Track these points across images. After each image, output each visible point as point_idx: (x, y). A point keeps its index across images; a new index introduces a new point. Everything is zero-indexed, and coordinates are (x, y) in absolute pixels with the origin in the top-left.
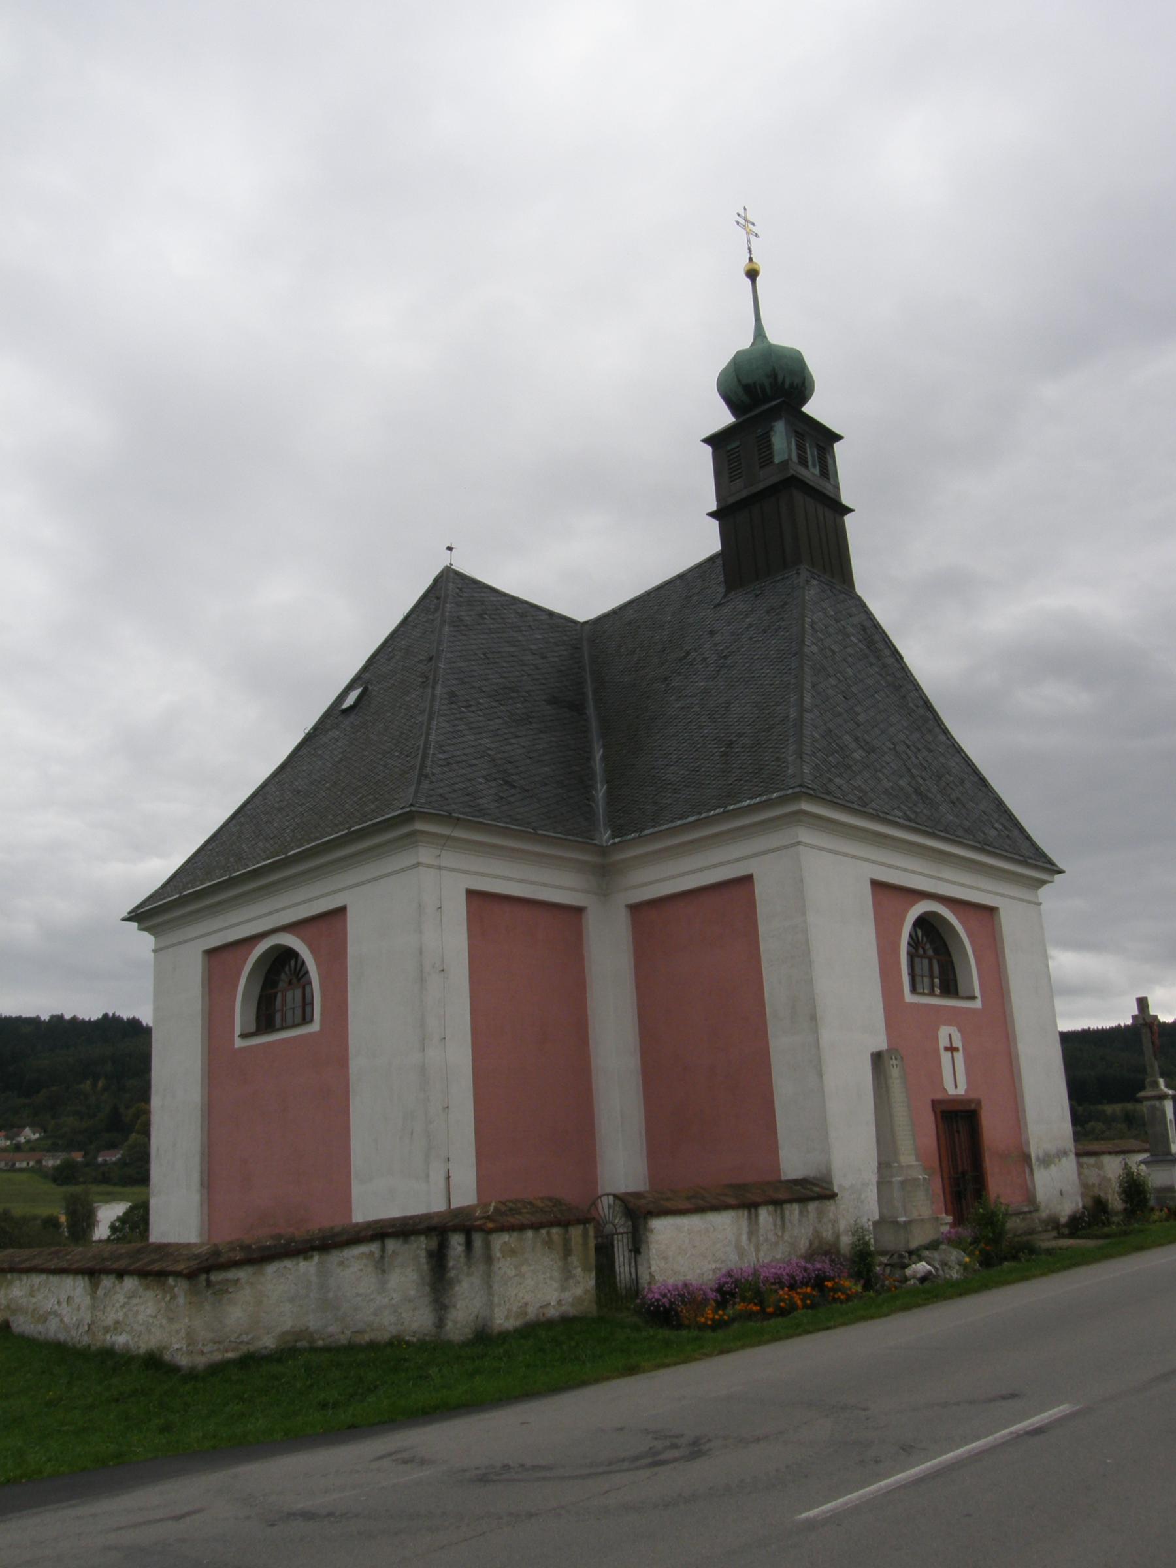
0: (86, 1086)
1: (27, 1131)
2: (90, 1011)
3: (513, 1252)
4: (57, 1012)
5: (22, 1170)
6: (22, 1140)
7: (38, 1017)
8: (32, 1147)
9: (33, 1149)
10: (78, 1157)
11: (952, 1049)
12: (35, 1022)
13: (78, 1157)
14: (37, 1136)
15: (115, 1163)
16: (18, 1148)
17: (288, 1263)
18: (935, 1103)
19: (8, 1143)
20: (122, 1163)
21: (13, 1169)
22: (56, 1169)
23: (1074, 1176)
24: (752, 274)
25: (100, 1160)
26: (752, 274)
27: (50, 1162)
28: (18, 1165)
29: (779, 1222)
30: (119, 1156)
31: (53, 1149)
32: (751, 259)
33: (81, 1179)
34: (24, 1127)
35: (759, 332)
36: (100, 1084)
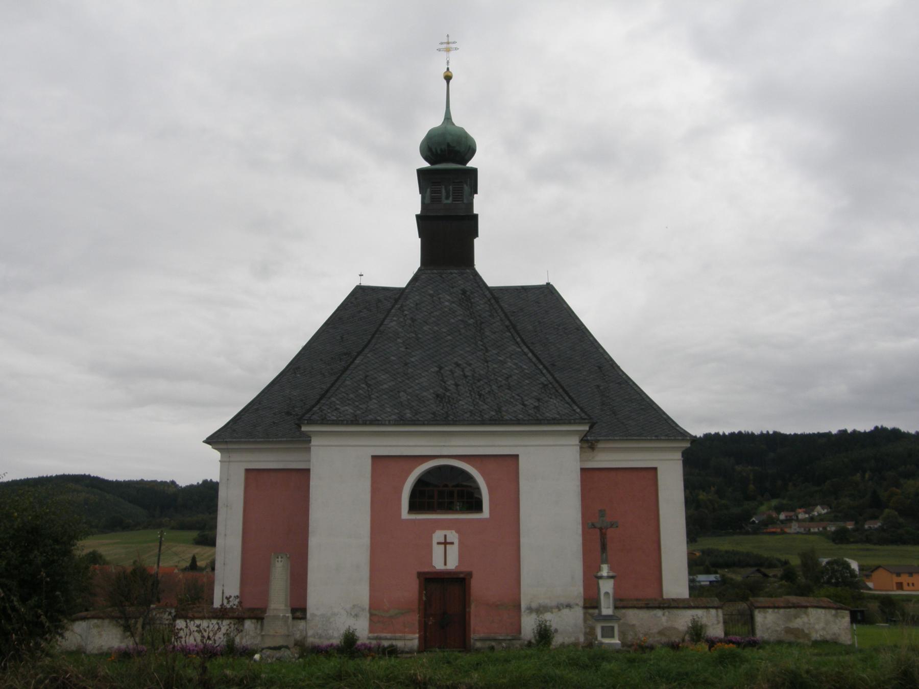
0: (858, 477)
1: (819, 508)
2: (865, 426)
3: (98, 626)
4: (842, 428)
5: (815, 533)
6: (816, 513)
7: (830, 432)
8: (821, 518)
9: (822, 520)
10: (850, 526)
11: (445, 543)
12: (828, 435)
13: (850, 526)
14: (825, 511)
15: (876, 529)
16: (812, 519)
17: (80, 622)
18: (420, 575)
19: (807, 516)
20: (881, 529)
21: (809, 533)
22: (833, 533)
23: (580, 621)
24: (448, 78)
25: (866, 527)
26: (448, 78)
27: (832, 528)
28: (812, 530)
29: (259, 627)
30: (879, 524)
31: (835, 519)
32: (448, 69)
33: (852, 540)
34: (817, 505)
35: (448, 118)
36: (867, 476)
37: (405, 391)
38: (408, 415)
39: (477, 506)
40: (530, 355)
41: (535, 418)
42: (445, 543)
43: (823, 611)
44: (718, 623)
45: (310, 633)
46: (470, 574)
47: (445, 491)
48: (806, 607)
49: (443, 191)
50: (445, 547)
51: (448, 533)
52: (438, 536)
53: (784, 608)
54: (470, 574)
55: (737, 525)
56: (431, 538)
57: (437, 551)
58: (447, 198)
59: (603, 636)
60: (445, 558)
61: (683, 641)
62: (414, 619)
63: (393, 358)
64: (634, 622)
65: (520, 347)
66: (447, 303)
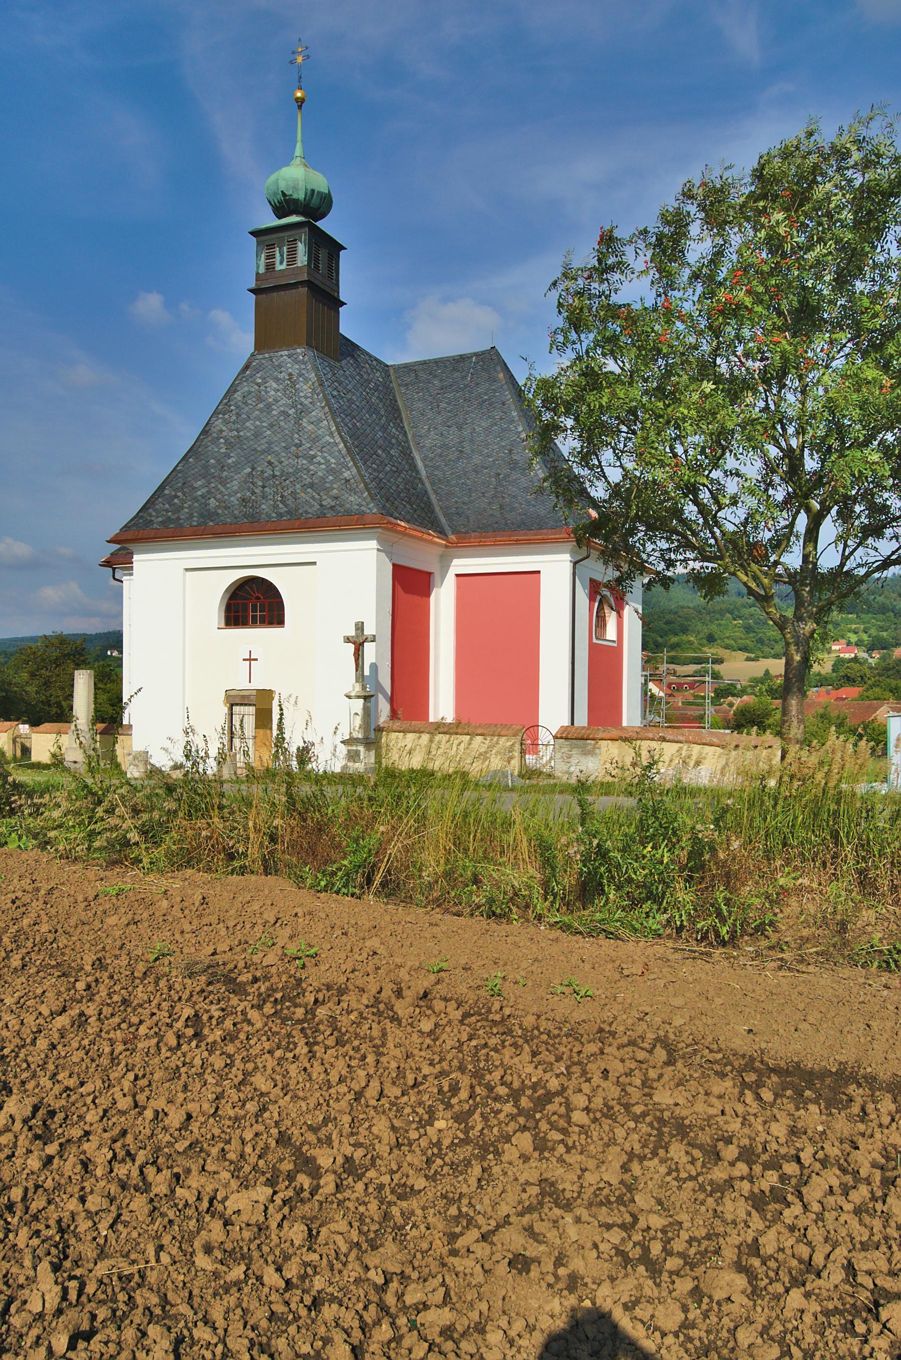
40: (342, 445)
63: (212, 461)
66: (273, 393)
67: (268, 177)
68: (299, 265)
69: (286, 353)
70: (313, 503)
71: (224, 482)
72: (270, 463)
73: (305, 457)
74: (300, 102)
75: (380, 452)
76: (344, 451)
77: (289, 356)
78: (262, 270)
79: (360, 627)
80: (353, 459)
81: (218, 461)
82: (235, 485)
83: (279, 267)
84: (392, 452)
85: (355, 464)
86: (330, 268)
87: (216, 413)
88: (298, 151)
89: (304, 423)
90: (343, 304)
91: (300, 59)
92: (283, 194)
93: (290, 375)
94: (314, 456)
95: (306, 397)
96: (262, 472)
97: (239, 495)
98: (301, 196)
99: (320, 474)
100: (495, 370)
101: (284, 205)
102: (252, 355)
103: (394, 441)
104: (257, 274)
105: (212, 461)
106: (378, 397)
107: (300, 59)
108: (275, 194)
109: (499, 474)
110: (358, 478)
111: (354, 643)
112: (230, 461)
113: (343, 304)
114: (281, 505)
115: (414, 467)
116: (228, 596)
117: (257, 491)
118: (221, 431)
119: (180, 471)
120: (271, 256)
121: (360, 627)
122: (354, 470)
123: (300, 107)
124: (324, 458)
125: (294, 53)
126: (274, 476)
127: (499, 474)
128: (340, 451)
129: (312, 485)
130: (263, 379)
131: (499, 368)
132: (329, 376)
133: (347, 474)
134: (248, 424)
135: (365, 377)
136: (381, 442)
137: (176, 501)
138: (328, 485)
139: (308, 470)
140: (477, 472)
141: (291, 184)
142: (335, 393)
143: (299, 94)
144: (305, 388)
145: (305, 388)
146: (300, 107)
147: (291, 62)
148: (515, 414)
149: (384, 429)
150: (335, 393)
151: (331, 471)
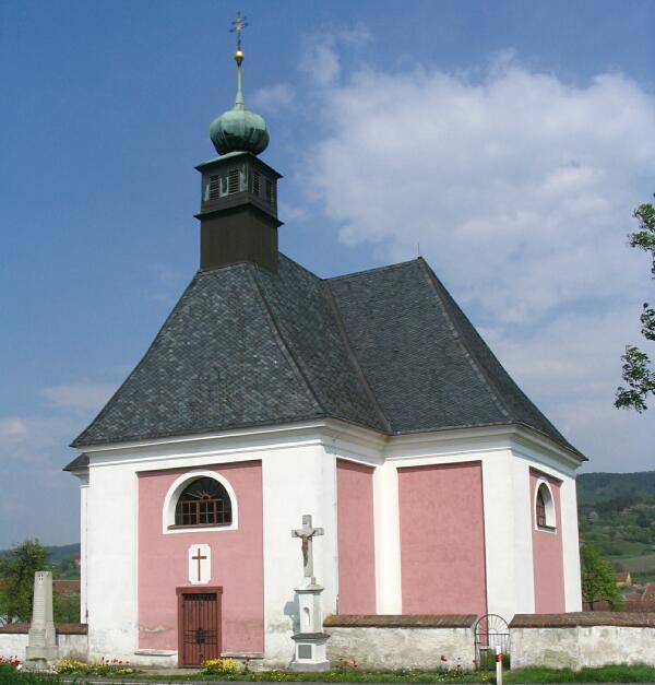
37: (164, 403)
38: (161, 428)
39: (227, 519)
40: (283, 348)
41: (275, 419)
42: (199, 558)
43: (639, 629)
44: (467, 644)
45: (91, 647)
46: (220, 589)
47: (203, 504)
48: (574, 626)
49: (221, 185)
50: (201, 559)
51: (201, 546)
52: (193, 551)
53: (545, 626)
54: (220, 589)
55: (588, 530)
56: (187, 552)
57: (193, 564)
58: (224, 191)
59: (300, 657)
60: (200, 575)
61: (294, 659)
62: (174, 634)
63: (162, 370)
64: (375, 642)
65: (275, 341)
66: (217, 304)
67: (212, 120)
68: (241, 190)
69: (229, 268)
70: (258, 403)
71: (172, 388)
72: (216, 369)
73: (249, 360)
74: (239, 61)
75: (320, 354)
76: (286, 353)
77: (233, 271)
78: (207, 198)
79: (307, 520)
80: (295, 360)
81: (167, 369)
82: (183, 391)
83: (222, 195)
84: (331, 355)
85: (297, 364)
86: (268, 193)
87: (165, 326)
88: (239, 98)
89: (248, 328)
90: (281, 224)
91: (239, 28)
92: (226, 133)
93: (234, 288)
94: (257, 360)
95: (249, 306)
96: (209, 377)
97: (187, 400)
98: (242, 134)
99: (264, 375)
100: (424, 277)
101: (225, 141)
102: (199, 273)
103: (332, 345)
104: (203, 202)
105: (162, 370)
106: (315, 307)
107: (239, 28)
108: (219, 133)
109: (434, 371)
110: (300, 376)
111: (302, 537)
112: (178, 369)
113: (281, 224)
114: (227, 407)
115: (352, 368)
116: (180, 493)
117: (203, 395)
118: (171, 342)
119: (132, 382)
120: (214, 187)
121: (307, 520)
122: (296, 370)
123: (239, 64)
124: (267, 360)
125: (234, 23)
126: (220, 380)
127: (434, 371)
128: (282, 353)
129: (256, 387)
130: (208, 292)
131: (427, 275)
132: (270, 287)
133: (289, 374)
134: (194, 334)
135: (303, 288)
136: (320, 346)
137: (128, 408)
138: (271, 385)
139: (252, 372)
140: (412, 370)
141: (232, 124)
142: (276, 301)
143: (239, 54)
144: (247, 298)
145: (247, 298)
146: (239, 64)
147: (239, 13)
148: (445, 314)
149: (322, 334)
150: (276, 301)
151: (274, 372)
